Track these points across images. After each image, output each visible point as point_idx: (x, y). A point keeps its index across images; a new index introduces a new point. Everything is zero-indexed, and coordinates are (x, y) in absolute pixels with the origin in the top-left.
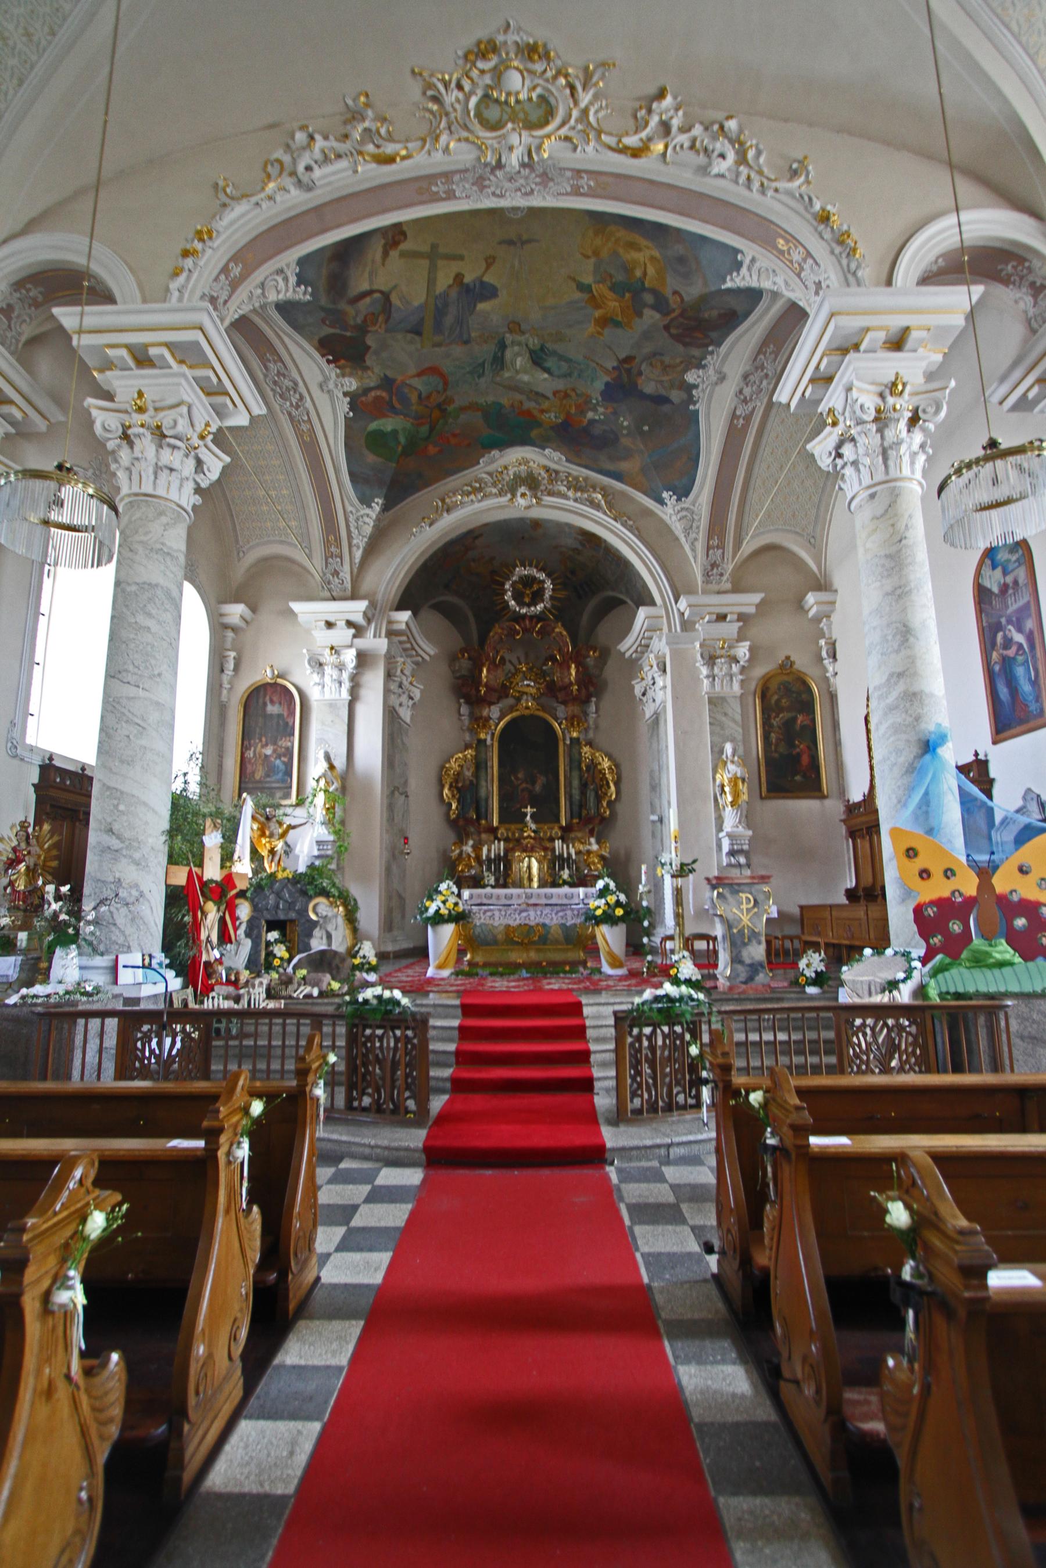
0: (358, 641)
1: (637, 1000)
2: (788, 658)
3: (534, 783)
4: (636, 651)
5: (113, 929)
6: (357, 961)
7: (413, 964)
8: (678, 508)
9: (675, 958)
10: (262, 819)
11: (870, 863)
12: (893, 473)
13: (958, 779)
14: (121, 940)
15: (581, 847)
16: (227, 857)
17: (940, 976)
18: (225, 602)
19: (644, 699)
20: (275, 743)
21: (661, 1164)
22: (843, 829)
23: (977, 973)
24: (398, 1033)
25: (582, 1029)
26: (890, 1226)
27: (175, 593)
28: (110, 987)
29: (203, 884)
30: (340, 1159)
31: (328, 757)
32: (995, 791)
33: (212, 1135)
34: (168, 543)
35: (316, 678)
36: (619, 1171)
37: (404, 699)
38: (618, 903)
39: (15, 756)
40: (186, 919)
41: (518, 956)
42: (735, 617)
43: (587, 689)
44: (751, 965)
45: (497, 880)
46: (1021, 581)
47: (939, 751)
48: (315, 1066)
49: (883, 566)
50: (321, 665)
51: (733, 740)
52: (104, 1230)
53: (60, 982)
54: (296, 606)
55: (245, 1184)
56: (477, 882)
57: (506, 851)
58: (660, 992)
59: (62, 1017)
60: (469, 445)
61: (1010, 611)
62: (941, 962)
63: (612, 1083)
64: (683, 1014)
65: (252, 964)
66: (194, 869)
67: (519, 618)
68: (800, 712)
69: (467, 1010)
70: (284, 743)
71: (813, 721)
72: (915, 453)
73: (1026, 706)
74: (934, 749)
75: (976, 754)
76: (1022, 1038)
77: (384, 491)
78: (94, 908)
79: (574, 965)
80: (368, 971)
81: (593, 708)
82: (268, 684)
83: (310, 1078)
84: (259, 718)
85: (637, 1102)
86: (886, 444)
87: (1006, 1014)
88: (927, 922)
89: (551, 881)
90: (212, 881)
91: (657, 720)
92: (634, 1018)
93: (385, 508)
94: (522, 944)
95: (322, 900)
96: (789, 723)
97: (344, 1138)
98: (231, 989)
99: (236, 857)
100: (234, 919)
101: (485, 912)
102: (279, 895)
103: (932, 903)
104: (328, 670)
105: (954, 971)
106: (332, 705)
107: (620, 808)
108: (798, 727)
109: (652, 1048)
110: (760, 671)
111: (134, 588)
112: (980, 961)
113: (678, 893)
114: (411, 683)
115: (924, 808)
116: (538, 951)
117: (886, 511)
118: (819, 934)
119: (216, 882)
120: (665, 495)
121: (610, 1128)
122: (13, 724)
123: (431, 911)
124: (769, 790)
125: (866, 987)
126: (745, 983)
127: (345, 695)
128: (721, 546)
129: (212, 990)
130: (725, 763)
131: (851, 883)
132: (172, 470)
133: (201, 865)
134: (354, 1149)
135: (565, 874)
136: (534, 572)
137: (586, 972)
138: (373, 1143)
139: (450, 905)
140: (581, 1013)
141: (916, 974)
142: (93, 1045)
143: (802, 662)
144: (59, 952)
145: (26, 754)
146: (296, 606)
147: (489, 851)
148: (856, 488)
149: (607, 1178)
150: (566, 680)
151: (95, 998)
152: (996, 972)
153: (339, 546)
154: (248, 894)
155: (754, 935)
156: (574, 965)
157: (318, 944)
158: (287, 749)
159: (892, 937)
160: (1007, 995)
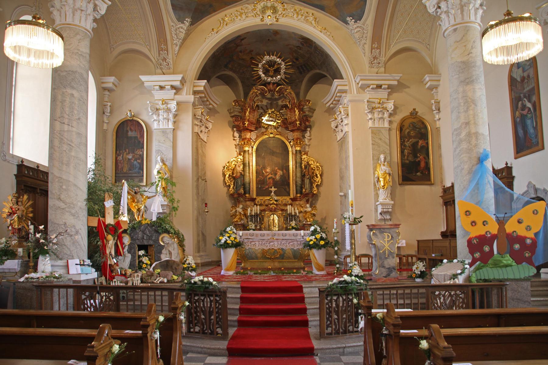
0: (179, 98)
1: (330, 283)
2: (414, 109)
3: (276, 174)
4: (332, 103)
5: (65, 247)
6: (185, 266)
7: (213, 269)
8: (355, 26)
9: (351, 265)
10: (133, 193)
11: (451, 218)
12: (466, 19)
13: (493, 177)
14: (69, 253)
15: (302, 209)
16: (117, 213)
17: (478, 272)
18: (104, 76)
19: (337, 130)
20: (133, 153)
21: (340, 355)
22: (441, 201)
23: (495, 270)
24: (212, 299)
25: (303, 298)
26: (421, 348)
27: (85, 76)
28: (66, 275)
29: (106, 226)
30: (187, 353)
31: (163, 161)
32: (515, 183)
33: (145, 327)
34: (81, 49)
35: (155, 117)
36: (320, 358)
37: (203, 128)
38: (322, 238)
39: (5, 160)
40: (99, 243)
42: (386, 86)
43: (305, 123)
44: (389, 268)
45: (256, 226)
46: (531, 76)
47: (485, 163)
48: (180, 306)
49: (460, 67)
50: (157, 110)
51: (384, 153)
52: (119, 351)
53: (43, 272)
54: (143, 78)
55: (159, 348)
56: (245, 228)
57: (261, 211)
58: (342, 279)
59: (46, 287)
61: (525, 91)
62: (479, 264)
63: (318, 323)
64: (352, 290)
65: (131, 266)
66: (101, 218)
67: (266, 84)
68: (421, 139)
69: (244, 289)
70: (139, 152)
71: (427, 143)
72: (478, 9)
73: (531, 140)
74: (482, 162)
75: (507, 164)
76: (513, 299)
78: (56, 237)
79: (298, 269)
80: (191, 271)
81: (307, 134)
82: (129, 120)
83: (178, 311)
84: (127, 139)
85: (330, 330)
86: (463, 3)
87: (506, 288)
88: (472, 247)
90: (110, 224)
91: (344, 139)
92: (328, 291)
93: (192, 24)
94: (270, 259)
95: (166, 235)
96: (415, 145)
97: (188, 344)
98: (123, 278)
99: (120, 213)
100: (122, 244)
101: (251, 242)
102: (143, 232)
103: (476, 237)
104: (161, 112)
105: (484, 269)
106: (164, 132)
107: (321, 189)
108: (419, 147)
109: (337, 305)
110: (398, 118)
111: (65, 74)
112: (497, 265)
113: (352, 233)
114: (207, 120)
115: (476, 191)
116: (280, 262)
117: (462, 38)
118: (426, 254)
119: (95, 227)
120: (348, 19)
121: (316, 341)
122: (3, 144)
123: (223, 241)
124: (403, 180)
125: (443, 277)
126: (385, 277)
127: (171, 126)
128: (379, 48)
129: (114, 278)
130: (380, 165)
131: (444, 229)
132: (82, 10)
133: (104, 217)
134: (193, 349)
135: (293, 223)
136: (273, 58)
137: (304, 273)
138: (202, 346)
139: (232, 238)
140: (302, 291)
141: (466, 271)
142: (63, 301)
143: (422, 112)
144: (41, 258)
145: (11, 159)
146: (143, 78)
147: (251, 210)
148: (447, 25)
149: (314, 361)
150: (293, 119)
151: (60, 280)
152: (504, 269)
153: (166, 44)
154: (128, 232)
155: (391, 253)
157: (164, 257)
158: (140, 155)
159: (458, 254)
160: (507, 280)
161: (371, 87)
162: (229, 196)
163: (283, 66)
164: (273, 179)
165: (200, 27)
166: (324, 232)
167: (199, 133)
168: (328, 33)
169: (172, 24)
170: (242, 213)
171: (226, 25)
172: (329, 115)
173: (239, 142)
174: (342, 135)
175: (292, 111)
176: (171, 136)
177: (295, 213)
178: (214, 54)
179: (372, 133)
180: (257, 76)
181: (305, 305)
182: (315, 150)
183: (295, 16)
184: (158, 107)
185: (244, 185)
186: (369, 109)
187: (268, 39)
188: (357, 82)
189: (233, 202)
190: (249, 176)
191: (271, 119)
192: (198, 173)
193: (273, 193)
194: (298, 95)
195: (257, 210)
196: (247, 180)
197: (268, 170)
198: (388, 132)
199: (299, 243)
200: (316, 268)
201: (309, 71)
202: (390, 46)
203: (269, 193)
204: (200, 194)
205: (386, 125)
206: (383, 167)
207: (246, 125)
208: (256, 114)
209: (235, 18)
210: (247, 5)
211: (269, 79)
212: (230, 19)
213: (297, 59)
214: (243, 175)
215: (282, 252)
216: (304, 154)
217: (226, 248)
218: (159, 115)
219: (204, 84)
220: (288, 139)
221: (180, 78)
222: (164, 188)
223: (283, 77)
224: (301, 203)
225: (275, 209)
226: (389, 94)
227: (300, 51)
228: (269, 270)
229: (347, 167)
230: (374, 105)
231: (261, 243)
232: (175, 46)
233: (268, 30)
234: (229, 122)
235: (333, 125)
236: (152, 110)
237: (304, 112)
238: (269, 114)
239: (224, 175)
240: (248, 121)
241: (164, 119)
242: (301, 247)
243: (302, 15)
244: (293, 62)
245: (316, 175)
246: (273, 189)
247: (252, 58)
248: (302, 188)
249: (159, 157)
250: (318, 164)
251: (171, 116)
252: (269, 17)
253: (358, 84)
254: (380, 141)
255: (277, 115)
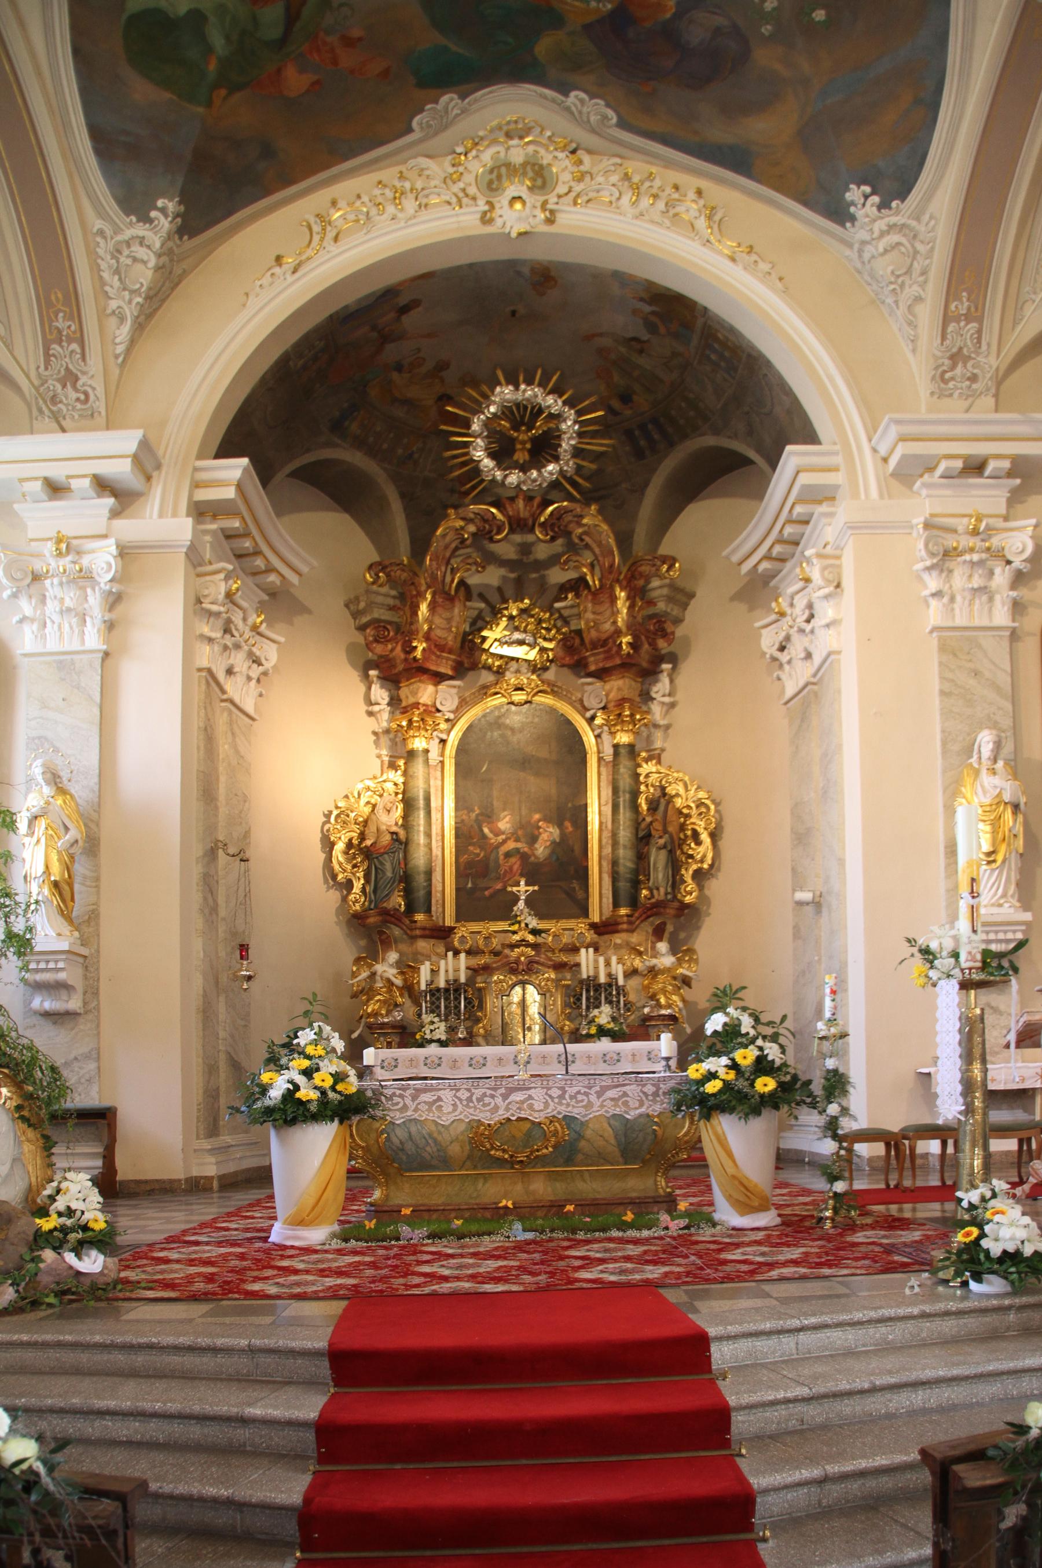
0: (130, 528)
3: (533, 839)
4: (768, 557)
8: (880, 225)
15: (637, 963)
19: (784, 657)
31: (54, 778)
35: (26, 607)
37: (239, 660)
38: (762, 1066)
41: (502, 1191)
45: (452, 1030)
50: (36, 577)
51: (994, 726)
56: (406, 1036)
57: (474, 971)
60: (386, 73)
77: (180, 181)
79: (645, 1206)
81: (661, 688)
89: (570, 1028)
91: (812, 697)
94: (511, 1163)
101: (419, 1091)
104: (51, 587)
106: (64, 664)
107: (714, 887)
114: (255, 628)
116: (552, 1176)
120: (854, 193)
123: (276, 1093)
127: (93, 639)
128: (975, 315)
130: (977, 773)
135: (604, 1015)
136: (529, 392)
137: (675, 1226)
139: (323, 1079)
147: (434, 972)
150: (607, 627)
153: (76, 314)
156: (645, 1206)
161: (940, 471)
162: (349, 923)
163: (569, 425)
164: (524, 857)
165: (224, 250)
166: (774, 1038)
167: (221, 676)
168: (764, 266)
169: (99, 224)
170: (398, 982)
171: (336, 239)
172: (751, 609)
173: (390, 721)
174: (811, 670)
175: (604, 597)
176: (93, 682)
177: (609, 975)
178: (284, 361)
179: (943, 648)
180: (464, 464)
181: (730, 1463)
182: (697, 741)
183: (626, 200)
184: (39, 566)
185: (406, 879)
186: (933, 555)
187: (506, 304)
188: (883, 451)
189: (363, 943)
190: (429, 846)
191: (517, 636)
192: (210, 828)
193: (521, 904)
194: (624, 541)
195: (457, 970)
196: (419, 858)
197: (505, 824)
198: (1006, 644)
199: (650, 1089)
200: (729, 1198)
201: (672, 445)
202: (1019, 308)
203: (502, 908)
204: (222, 912)
205: (1001, 616)
206: (986, 779)
207: (418, 654)
208: (459, 616)
209: (374, 212)
210: (423, 162)
211: (514, 478)
212: (352, 217)
213: (626, 398)
214: (401, 843)
215: (567, 1134)
216: (647, 760)
217: (291, 1122)
218: (43, 600)
219: (237, 474)
220: (583, 709)
221: (132, 447)
222: (56, 884)
223: (570, 467)
224: (634, 938)
225: (531, 962)
226: (1015, 498)
227: (642, 361)
228: (500, 1214)
229: (830, 792)
230: (951, 541)
231: (464, 1095)
232: (113, 321)
233: (512, 265)
234: (352, 650)
235: (768, 641)
236: (11, 578)
237: (651, 603)
238: (511, 618)
239: (328, 845)
240: (427, 638)
241: (65, 611)
242: (658, 1108)
243: (655, 197)
244: (610, 410)
245: (696, 835)
246: (523, 889)
247: (446, 398)
248: (636, 884)
249: (39, 762)
250: (702, 794)
251: (94, 601)
252: (518, 206)
253: (885, 460)
254: (972, 682)
255: (540, 621)
